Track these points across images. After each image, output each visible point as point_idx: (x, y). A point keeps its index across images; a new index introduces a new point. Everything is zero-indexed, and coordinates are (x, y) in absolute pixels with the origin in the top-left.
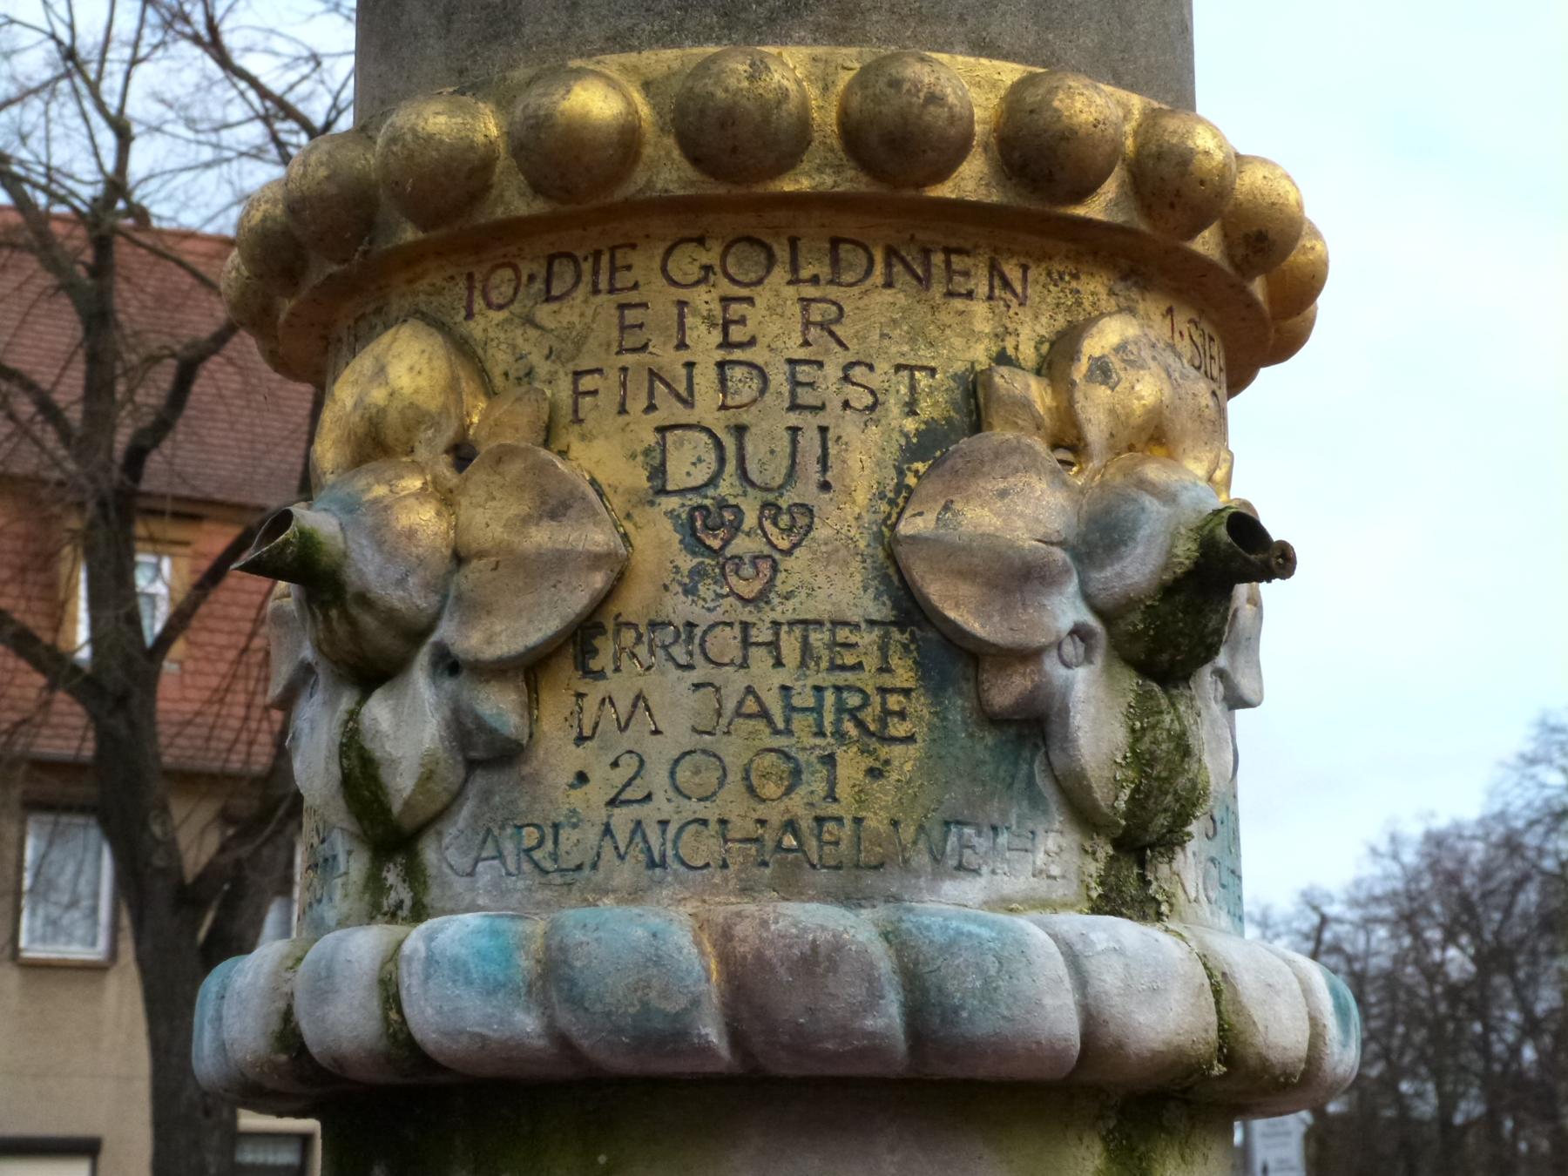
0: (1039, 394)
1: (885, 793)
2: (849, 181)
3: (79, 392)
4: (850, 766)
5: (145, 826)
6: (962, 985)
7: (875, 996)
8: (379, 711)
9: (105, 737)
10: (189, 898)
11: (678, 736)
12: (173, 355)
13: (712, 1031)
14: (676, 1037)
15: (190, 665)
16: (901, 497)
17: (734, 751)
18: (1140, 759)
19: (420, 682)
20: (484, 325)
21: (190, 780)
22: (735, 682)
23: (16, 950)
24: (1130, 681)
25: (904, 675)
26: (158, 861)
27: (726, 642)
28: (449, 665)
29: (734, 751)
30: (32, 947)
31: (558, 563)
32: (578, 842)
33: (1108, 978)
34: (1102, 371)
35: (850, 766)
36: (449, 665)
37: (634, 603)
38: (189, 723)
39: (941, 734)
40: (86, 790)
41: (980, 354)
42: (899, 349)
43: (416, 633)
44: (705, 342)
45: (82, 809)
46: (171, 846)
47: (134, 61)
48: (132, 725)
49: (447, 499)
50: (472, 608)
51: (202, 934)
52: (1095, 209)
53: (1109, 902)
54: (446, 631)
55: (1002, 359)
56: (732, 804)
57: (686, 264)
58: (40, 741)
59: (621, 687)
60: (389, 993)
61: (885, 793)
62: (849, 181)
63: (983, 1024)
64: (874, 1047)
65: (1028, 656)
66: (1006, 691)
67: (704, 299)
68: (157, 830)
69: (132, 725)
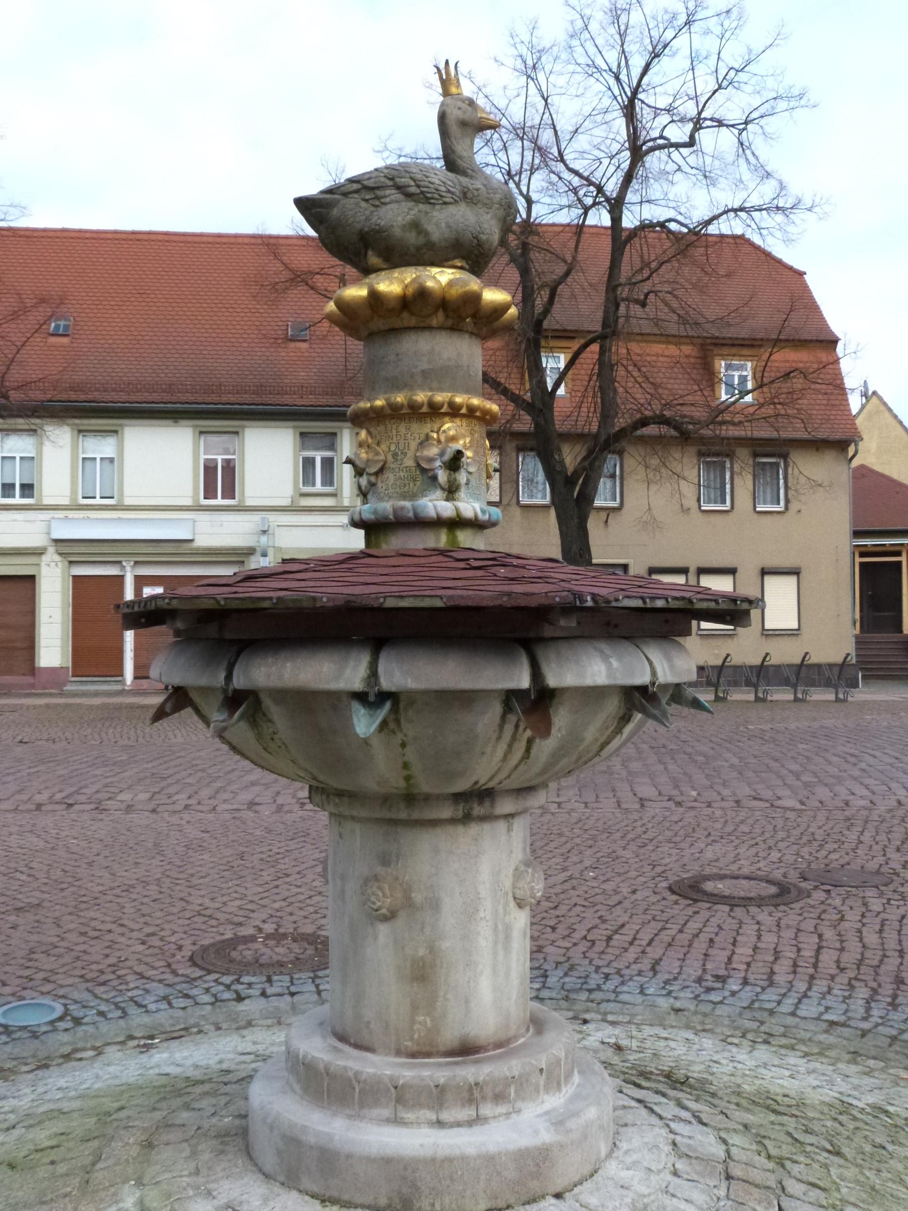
0: (435, 435)
1: (416, 488)
2: (409, 411)
3: (520, 298)
4: (412, 485)
5: (552, 456)
6: (419, 510)
7: (409, 512)
8: (361, 480)
9: (537, 425)
10: (570, 481)
11: (392, 481)
12: (548, 285)
13: (391, 517)
14: (386, 518)
15: (573, 394)
16: (417, 450)
17: (398, 483)
18: (449, 481)
19: (365, 476)
20: (372, 429)
21: (566, 437)
22: (398, 475)
23: (518, 501)
24: (448, 472)
25: (418, 473)
26: (558, 468)
27: (397, 470)
28: (368, 474)
29: (398, 483)
30: (524, 500)
31: (377, 461)
32: (382, 495)
33: (439, 509)
34: (444, 431)
35: (412, 485)
36: (368, 474)
37: (387, 466)
38: (569, 416)
39: (423, 480)
40: (532, 443)
41: (429, 431)
42: (418, 431)
43: (364, 470)
44: (394, 432)
45: (532, 450)
46: (562, 462)
47: (532, 174)
48: (545, 420)
49: (367, 453)
50: (369, 467)
51: (575, 494)
52: (443, 411)
53: (447, 500)
54: (367, 470)
55: (432, 431)
56: (398, 490)
57: (392, 421)
58: (514, 425)
59: (385, 476)
60: (360, 513)
61: (416, 488)
62: (409, 411)
63: (422, 515)
64: (410, 518)
65: (433, 470)
66: (430, 474)
67: (394, 426)
68: (557, 457)
69: (545, 420)
